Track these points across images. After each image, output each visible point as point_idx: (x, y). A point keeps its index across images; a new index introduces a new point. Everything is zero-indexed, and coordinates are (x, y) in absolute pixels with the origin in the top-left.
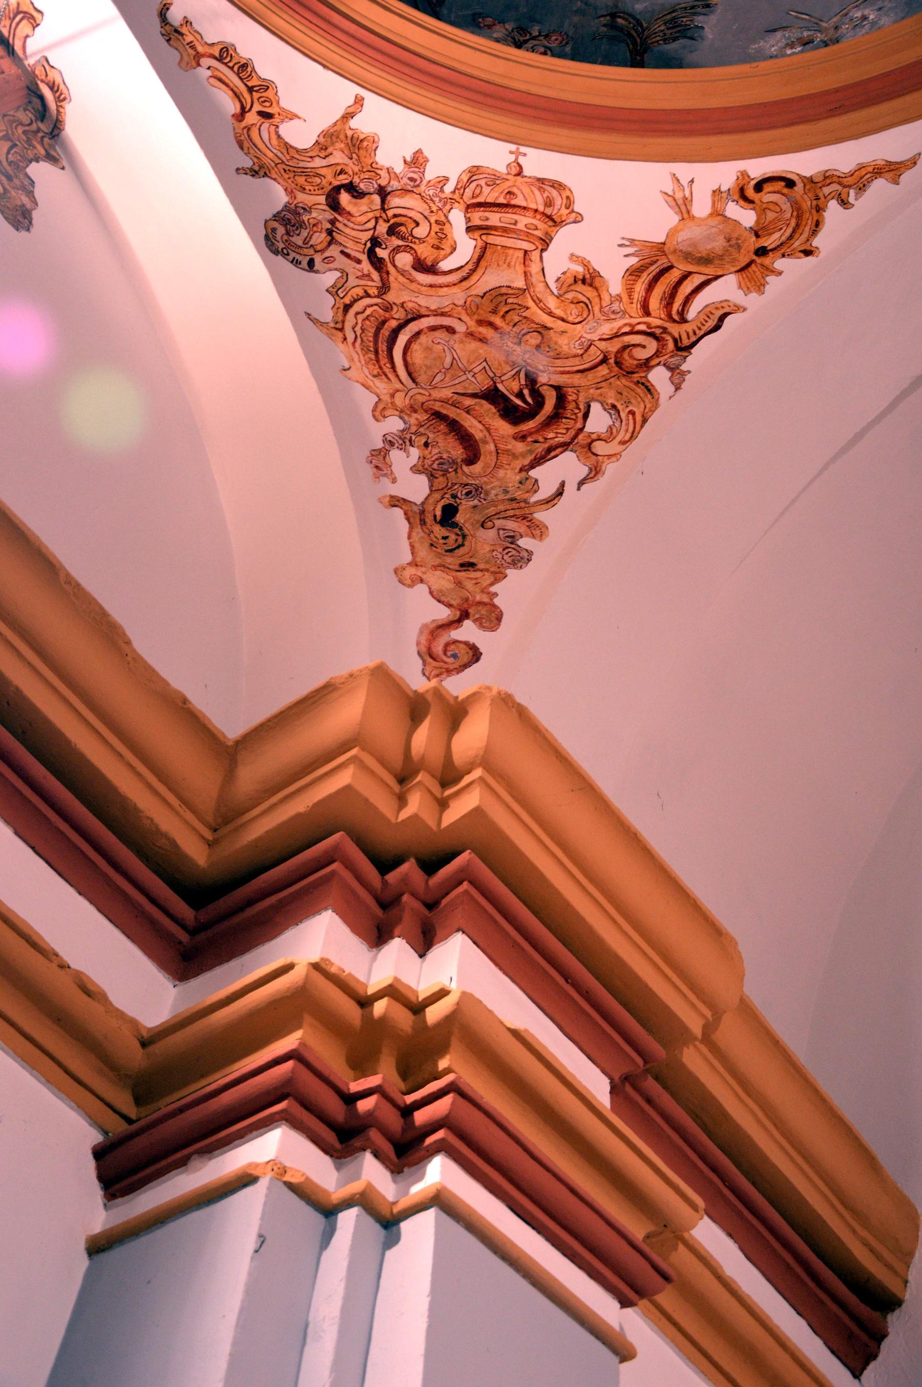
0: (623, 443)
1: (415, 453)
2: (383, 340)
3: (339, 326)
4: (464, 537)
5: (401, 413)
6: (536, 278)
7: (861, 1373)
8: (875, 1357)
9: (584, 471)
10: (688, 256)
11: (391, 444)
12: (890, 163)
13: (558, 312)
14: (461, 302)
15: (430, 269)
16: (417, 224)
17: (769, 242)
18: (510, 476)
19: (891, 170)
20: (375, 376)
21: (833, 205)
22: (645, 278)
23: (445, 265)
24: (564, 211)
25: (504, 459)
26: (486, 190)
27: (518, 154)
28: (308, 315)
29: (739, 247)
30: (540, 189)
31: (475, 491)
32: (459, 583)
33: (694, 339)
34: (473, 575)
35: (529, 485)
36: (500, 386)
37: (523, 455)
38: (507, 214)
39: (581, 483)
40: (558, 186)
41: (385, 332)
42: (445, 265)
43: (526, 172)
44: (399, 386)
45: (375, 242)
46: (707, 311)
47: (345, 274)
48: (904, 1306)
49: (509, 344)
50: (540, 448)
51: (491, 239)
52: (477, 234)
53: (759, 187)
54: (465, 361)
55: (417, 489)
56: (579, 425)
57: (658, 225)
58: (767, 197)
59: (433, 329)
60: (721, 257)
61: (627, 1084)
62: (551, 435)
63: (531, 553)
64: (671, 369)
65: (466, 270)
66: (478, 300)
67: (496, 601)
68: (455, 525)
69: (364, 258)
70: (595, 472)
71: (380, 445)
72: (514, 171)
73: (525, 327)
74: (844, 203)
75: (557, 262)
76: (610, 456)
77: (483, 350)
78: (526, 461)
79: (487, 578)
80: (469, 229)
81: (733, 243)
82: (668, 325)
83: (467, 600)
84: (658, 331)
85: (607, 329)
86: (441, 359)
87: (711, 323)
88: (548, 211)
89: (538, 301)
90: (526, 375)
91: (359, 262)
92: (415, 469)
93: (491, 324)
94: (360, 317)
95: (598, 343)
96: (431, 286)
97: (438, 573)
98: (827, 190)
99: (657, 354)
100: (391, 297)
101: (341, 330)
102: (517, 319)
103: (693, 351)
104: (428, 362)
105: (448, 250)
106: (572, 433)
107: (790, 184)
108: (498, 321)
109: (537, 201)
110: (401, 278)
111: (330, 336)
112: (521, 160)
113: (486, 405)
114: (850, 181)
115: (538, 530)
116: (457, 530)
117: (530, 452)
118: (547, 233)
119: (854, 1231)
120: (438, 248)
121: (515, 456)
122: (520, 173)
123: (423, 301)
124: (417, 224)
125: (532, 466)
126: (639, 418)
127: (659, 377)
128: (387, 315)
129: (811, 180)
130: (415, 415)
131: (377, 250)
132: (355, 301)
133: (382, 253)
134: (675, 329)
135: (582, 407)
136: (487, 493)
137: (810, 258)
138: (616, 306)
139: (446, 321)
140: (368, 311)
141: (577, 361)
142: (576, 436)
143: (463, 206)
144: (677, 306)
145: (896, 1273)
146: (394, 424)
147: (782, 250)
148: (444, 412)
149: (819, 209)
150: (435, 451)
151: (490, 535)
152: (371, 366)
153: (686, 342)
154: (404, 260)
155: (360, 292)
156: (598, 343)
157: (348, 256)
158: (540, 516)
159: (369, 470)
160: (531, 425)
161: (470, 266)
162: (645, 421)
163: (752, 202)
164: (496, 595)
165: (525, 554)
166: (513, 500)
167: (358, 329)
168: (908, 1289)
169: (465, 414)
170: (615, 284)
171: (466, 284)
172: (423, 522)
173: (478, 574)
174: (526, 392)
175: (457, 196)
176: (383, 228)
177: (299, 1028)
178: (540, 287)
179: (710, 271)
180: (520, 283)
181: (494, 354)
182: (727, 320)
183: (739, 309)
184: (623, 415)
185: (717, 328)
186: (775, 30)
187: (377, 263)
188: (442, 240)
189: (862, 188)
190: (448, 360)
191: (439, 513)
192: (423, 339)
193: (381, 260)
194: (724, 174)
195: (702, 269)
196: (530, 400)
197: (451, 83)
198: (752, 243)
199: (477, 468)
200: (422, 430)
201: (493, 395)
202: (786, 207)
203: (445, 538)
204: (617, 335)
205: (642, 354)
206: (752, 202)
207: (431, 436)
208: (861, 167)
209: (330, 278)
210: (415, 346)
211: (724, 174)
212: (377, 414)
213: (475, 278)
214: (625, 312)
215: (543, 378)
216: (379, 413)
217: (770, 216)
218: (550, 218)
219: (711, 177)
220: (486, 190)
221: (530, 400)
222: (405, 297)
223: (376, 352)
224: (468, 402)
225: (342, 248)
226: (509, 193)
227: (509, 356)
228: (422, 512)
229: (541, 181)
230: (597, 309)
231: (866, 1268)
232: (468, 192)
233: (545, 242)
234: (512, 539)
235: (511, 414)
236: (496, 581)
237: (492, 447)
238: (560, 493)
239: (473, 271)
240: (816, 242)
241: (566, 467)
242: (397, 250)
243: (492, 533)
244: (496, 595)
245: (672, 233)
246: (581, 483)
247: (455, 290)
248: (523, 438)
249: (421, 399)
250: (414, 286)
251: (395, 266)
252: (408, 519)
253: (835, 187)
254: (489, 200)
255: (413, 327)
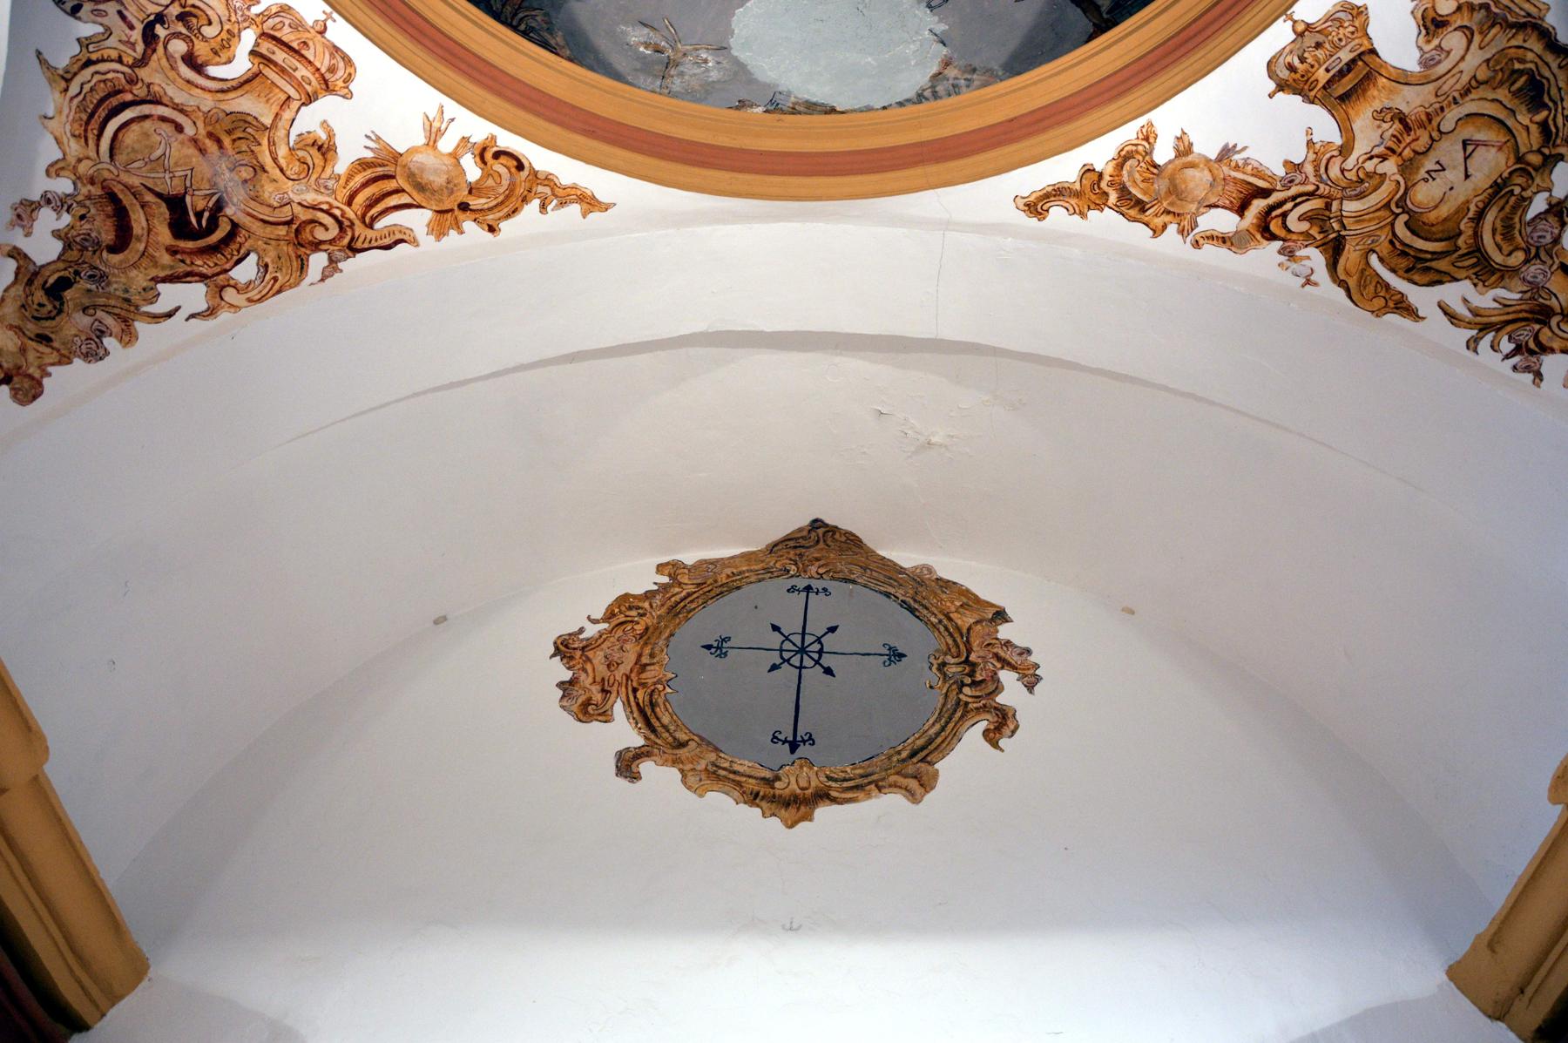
0: (250, 300)
1: (66, 219)
2: (104, 107)
3: (68, 76)
4: (60, 312)
5: (77, 179)
6: (283, 123)
9: (202, 306)
10: (411, 176)
11: (49, 202)
12: (593, 197)
13: (282, 162)
14: (205, 109)
15: (198, 68)
16: (210, 23)
17: (475, 203)
18: (139, 279)
19: (590, 203)
20: (74, 136)
21: (536, 203)
22: (369, 174)
23: (213, 71)
24: (340, 83)
25: (145, 262)
26: (287, 29)
27: (329, 16)
28: (39, 54)
29: (452, 192)
30: (331, 54)
31: (100, 278)
32: (23, 350)
33: (366, 245)
34: (42, 348)
35: (151, 294)
36: (188, 199)
37: (163, 268)
39: (193, 316)
40: (348, 61)
41: (114, 101)
42: (213, 71)
43: (327, 35)
44: (93, 154)
45: (160, 18)
46: (391, 229)
47: (109, 32)
49: (223, 166)
50: (182, 268)
51: (267, 71)
52: (257, 60)
53: (497, 155)
54: (172, 162)
55: (44, 247)
56: (227, 266)
57: (405, 137)
58: (498, 167)
59: (163, 119)
60: (434, 192)
62: (199, 262)
63: (107, 353)
64: (331, 260)
65: (229, 85)
66: (222, 115)
67: (46, 381)
68: (60, 299)
69: (139, 27)
70: (211, 312)
71: (36, 197)
72: (318, 28)
73: (246, 159)
74: (543, 207)
75: (308, 120)
76: (231, 306)
77: (196, 158)
78: (162, 274)
79: (55, 357)
80: (253, 53)
81: (450, 186)
82: (357, 222)
83: (20, 368)
84: (346, 223)
85: (310, 197)
86: (152, 148)
87: (387, 241)
88: (328, 76)
89: (272, 143)
90: (218, 201)
91: (132, 27)
92: (56, 234)
93: (219, 141)
94: (97, 78)
95: (295, 206)
96: (188, 82)
97: (11, 333)
98: (540, 189)
99: (332, 242)
100: (143, 73)
101: (68, 81)
102: (244, 148)
103: (359, 256)
104: (137, 146)
105: (224, 59)
106: (218, 269)
107: (520, 167)
108: (227, 141)
109: (323, 63)
110: (164, 62)
111: (51, 82)
112: (329, 23)
113: (164, 209)
114: (560, 192)
115: (128, 336)
116: (57, 304)
117: (172, 267)
118: (315, 92)
119: (71, 971)
120: (216, 53)
121: (156, 265)
122: (322, 33)
123: (171, 91)
124: (210, 23)
125: (164, 280)
126: (277, 287)
127: (318, 261)
128: (127, 87)
129: (535, 173)
130: (90, 187)
131: (158, 26)
132: (103, 60)
133: (160, 31)
134: (359, 229)
135: (242, 251)
136: (109, 284)
137: (490, 235)
138: (330, 183)
139: (180, 119)
140: (110, 76)
141: (267, 210)
142: (218, 274)
143: (259, 31)
144: (374, 211)
146: (64, 186)
147: (478, 215)
148: (121, 196)
149: (525, 200)
150: (87, 226)
151: (84, 321)
152: (76, 125)
153: (359, 245)
154: (178, 47)
155: (114, 55)
156: (295, 206)
157: (123, 17)
158: (140, 326)
159: (9, 215)
160: (190, 245)
161: (234, 83)
162: (279, 291)
163: (485, 163)
164: (49, 375)
165: (101, 352)
166: (127, 300)
167: (87, 88)
169: (138, 207)
170: (342, 166)
171: (220, 96)
172: (30, 282)
173: (48, 350)
174: (206, 214)
175: (258, 20)
176: (175, 10)
178: (281, 133)
179: (419, 198)
180: (267, 121)
181: (203, 167)
182: (400, 246)
183: (414, 242)
184: (268, 277)
185: (388, 247)
186: (645, 25)
187: (149, 37)
188: (223, 50)
189: (562, 204)
190: (159, 153)
191: (51, 281)
192: (147, 124)
193: (156, 37)
194: (479, 129)
195: (415, 194)
196: (204, 223)
198: (462, 195)
199: (115, 259)
200: (88, 203)
201: (176, 204)
202: (505, 183)
203: (40, 305)
204: (314, 208)
205: (321, 235)
206: (485, 163)
207: (93, 211)
208: (574, 187)
209: (88, 29)
210: (134, 127)
211: (479, 129)
212: (53, 170)
213: (231, 95)
214: (334, 192)
215: (229, 211)
216: (54, 170)
217: (490, 182)
218: (326, 82)
219: (472, 126)
220: (287, 29)
221: (204, 223)
222: (157, 79)
223: (91, 116)
224: (149, 198)
225: (119, 7)
226: (305, 43)
227: (220, 175)
228: (36, 274)
229: (337, 49)
230: (314, 177)
232: (271, 22)
233: (310, 99)
234: (101, 334)
235: (180, 227)
236: (60, 363)
237: (141, 247)
238: (169, 315)
239: (235, 89)
240: (504, 225)
241: (193, 295)
242: (177, 35)
243: (87, 320)
244: (49, 375)
245: (413, 150)
246: (193, 316)
247: (208, 96)
248: (173, 251)
249: (106, 175)
250: (172, 74)
251: (165, 48)
252: (17, 274)
253: (547, 190)
254: (285, 39)
255: (146, 109)
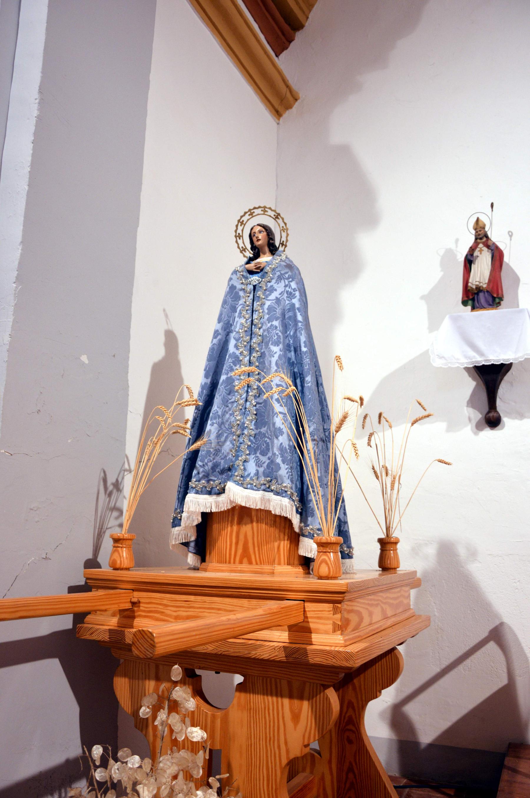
7: (279, 55)
8: (287, 48)
38: (278, 432)
48: (304, 28)
61: (297, 530)
145: (304, 12)
168: (308, 21)
177: (201, 777)
197: (22, 606)
231: (289, 6)
